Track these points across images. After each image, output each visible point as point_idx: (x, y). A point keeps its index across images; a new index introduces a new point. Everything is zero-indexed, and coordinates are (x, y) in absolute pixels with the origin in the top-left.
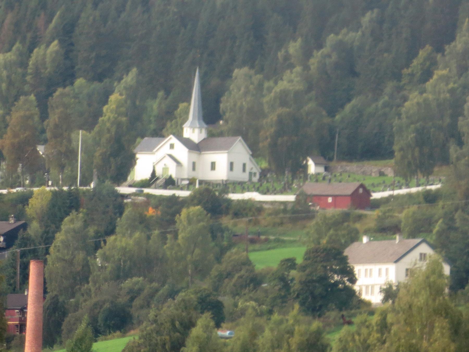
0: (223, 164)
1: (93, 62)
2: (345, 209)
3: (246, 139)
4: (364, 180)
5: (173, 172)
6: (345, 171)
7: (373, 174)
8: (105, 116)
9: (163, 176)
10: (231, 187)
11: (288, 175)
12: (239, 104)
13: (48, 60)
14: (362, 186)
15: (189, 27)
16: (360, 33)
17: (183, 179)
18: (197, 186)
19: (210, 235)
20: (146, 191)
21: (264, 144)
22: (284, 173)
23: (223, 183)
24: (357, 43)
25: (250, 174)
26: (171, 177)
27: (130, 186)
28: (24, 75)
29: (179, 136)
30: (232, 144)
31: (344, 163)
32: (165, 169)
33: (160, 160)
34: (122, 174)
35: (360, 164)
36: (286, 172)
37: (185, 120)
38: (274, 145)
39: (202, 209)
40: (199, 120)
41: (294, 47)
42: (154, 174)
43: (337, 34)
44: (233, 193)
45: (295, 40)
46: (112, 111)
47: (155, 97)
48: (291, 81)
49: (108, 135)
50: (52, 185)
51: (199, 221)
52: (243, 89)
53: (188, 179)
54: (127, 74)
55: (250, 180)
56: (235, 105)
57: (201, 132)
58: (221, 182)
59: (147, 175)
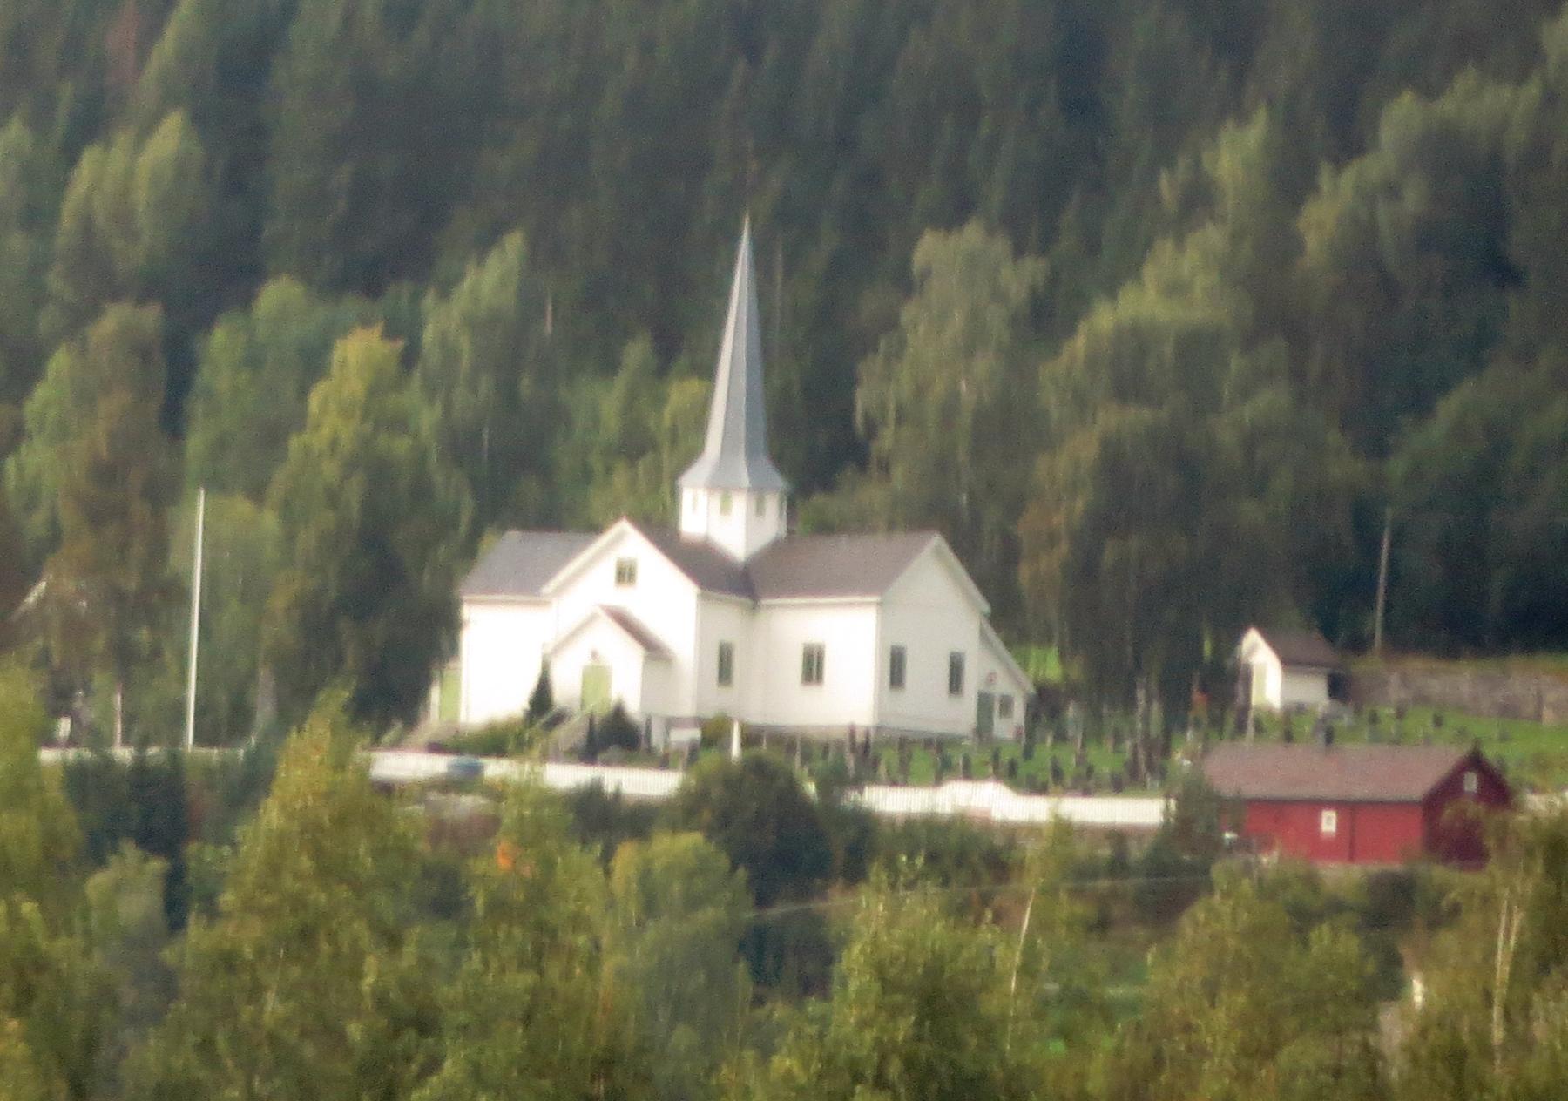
0: (861, 654)
1: (342, 205)
2: (1396, 867)
3: (965, 547)
4: (1504, 738)
5: (628, 688)
6: (1422, 699)
7: (1548, 714)
8: (317, 427)
9: (583, 705)
10: (889, 758)
11: (1149, 712)
12: (939, 389)
13: (142, 196)
14: (1475, 762)
15: (770, 56)
16: (1532, 90)
17: (671, 723)
18: (736, 749)
19: (742, 967)
20: (495, 769)
21: (1041, 570)
22: (1129, 702)
23: (853, 743)
24: (1517, 137)
25: (984, 702)
26: (618, 713)
27: (436, 748)
28: (37, 268)
29: (660, 527)
30: (899, 564)
31: (1416, 665)
32: (596, 675)
33: (572, 635)
34: (394, 690)
35: (1490, 667)
36: (1141, 695)
37: (691, 455)
38: (1084, 571)
39: (712, 847)
40: (751, 454)
41: (1235, 154)
42: (542, 699)
43: (1430, 92)
44: (894, 783)
45: (1243, 118)
46: (345, 413)
47: (609, 366)
48: (1171, 290)
49: (328, 519)
50: (72, 742)
51: (693, 902)
52: (958, 318)
53: (700, 722)
54: (481, 262)
55: (983, 728)
56: (920, 391)
57: (760, 510)
58: (846, 738)
59: (511, 703)
